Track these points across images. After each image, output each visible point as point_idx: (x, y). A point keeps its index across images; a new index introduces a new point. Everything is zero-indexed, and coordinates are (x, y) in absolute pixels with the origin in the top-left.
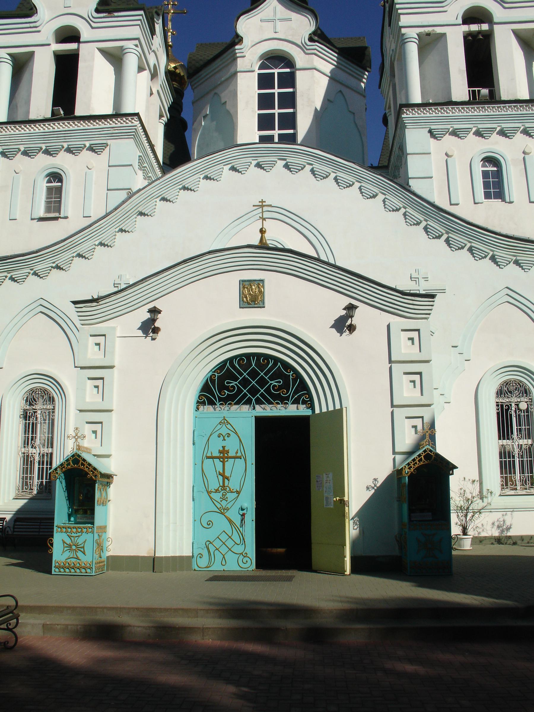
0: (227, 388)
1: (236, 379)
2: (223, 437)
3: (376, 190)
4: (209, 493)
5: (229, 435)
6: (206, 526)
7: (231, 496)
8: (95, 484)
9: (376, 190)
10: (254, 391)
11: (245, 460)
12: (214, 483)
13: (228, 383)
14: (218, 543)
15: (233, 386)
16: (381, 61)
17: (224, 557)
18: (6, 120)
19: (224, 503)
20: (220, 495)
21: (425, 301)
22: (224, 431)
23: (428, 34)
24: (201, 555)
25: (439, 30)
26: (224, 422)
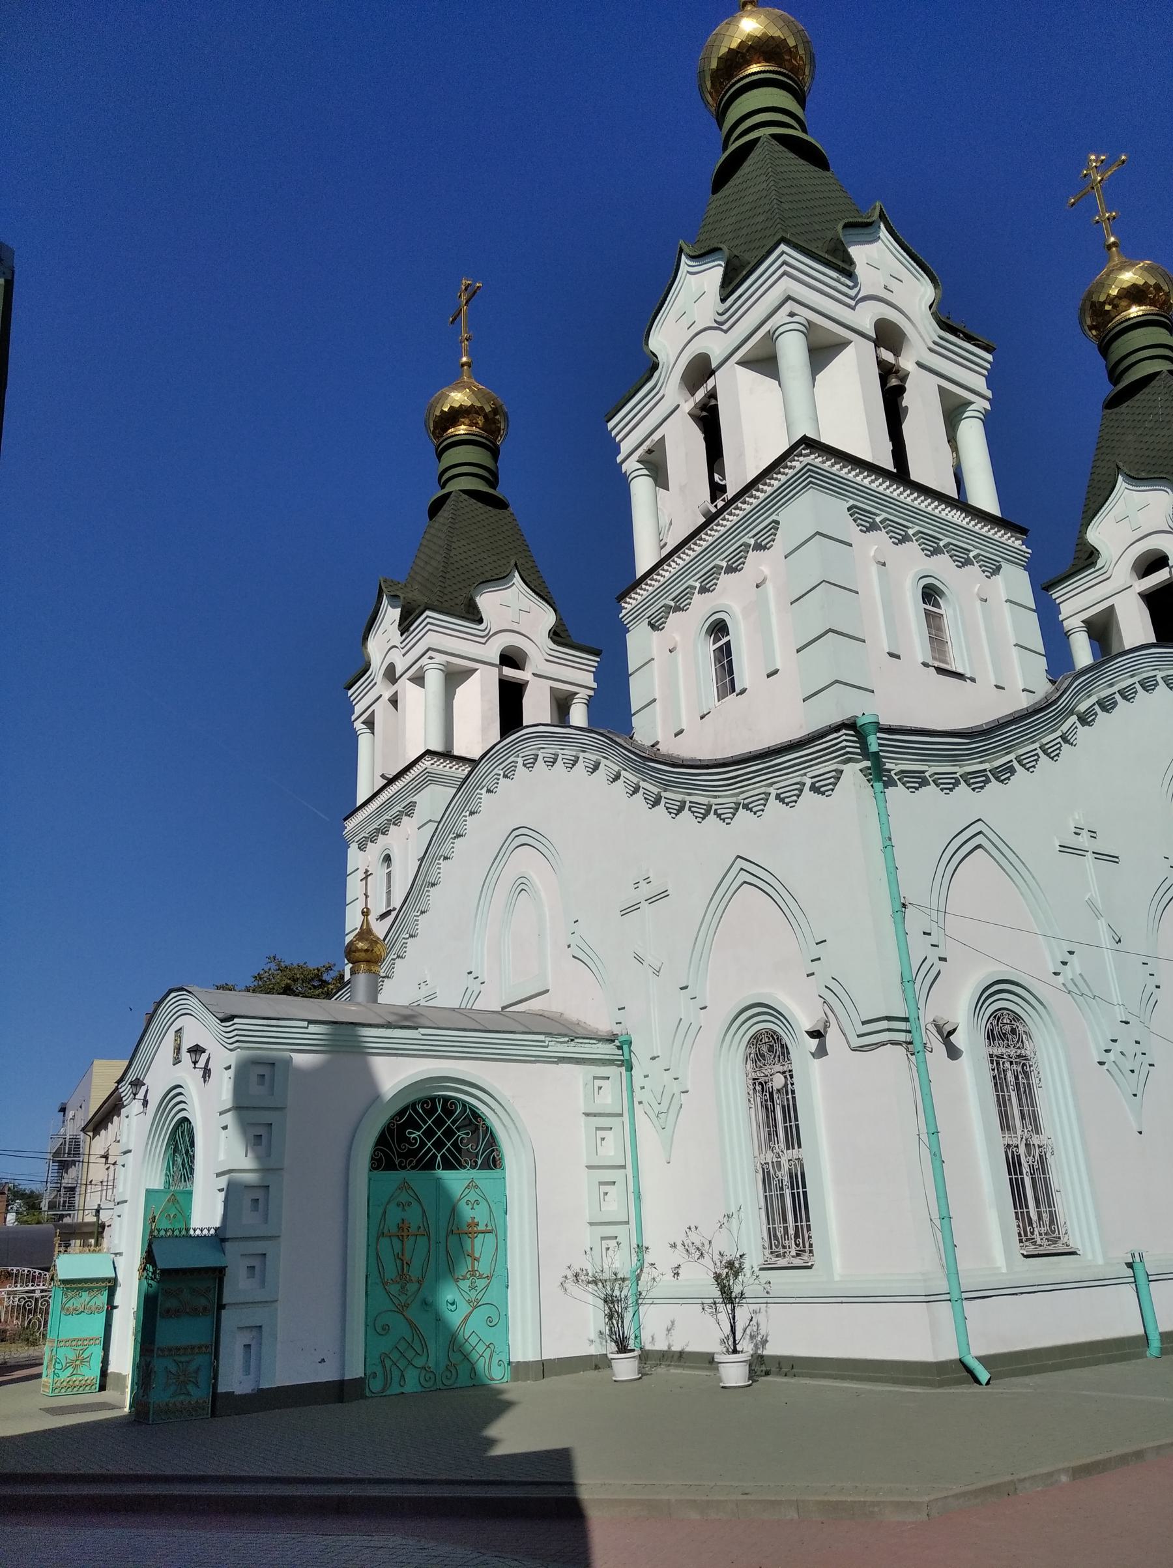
0: (408, 1140)
1: (418, 1128)
2: (402, 1206)
3: (832, 766)
4: (384, 1284)
5: (409, 1204)
6: (379, 1330)
7: (412, 1287)
8: (718, 69)
9: (832, 766)
10: (449, 1113)
11: (429, 1236)
12: (391, 1272)
13: (410, 1133)
14: (395, 1356)
15: (415, 1138)
16: (908, 428)
17: (403, 1376)
18: (111, 1369)
19: (403, 1298)
20: (398, 1287)
21: (1045, 580)
22: (404, 1197)
23: (650, 451)
24: (374, 1375)
25: (656, 437)
26: (405, 1186)
